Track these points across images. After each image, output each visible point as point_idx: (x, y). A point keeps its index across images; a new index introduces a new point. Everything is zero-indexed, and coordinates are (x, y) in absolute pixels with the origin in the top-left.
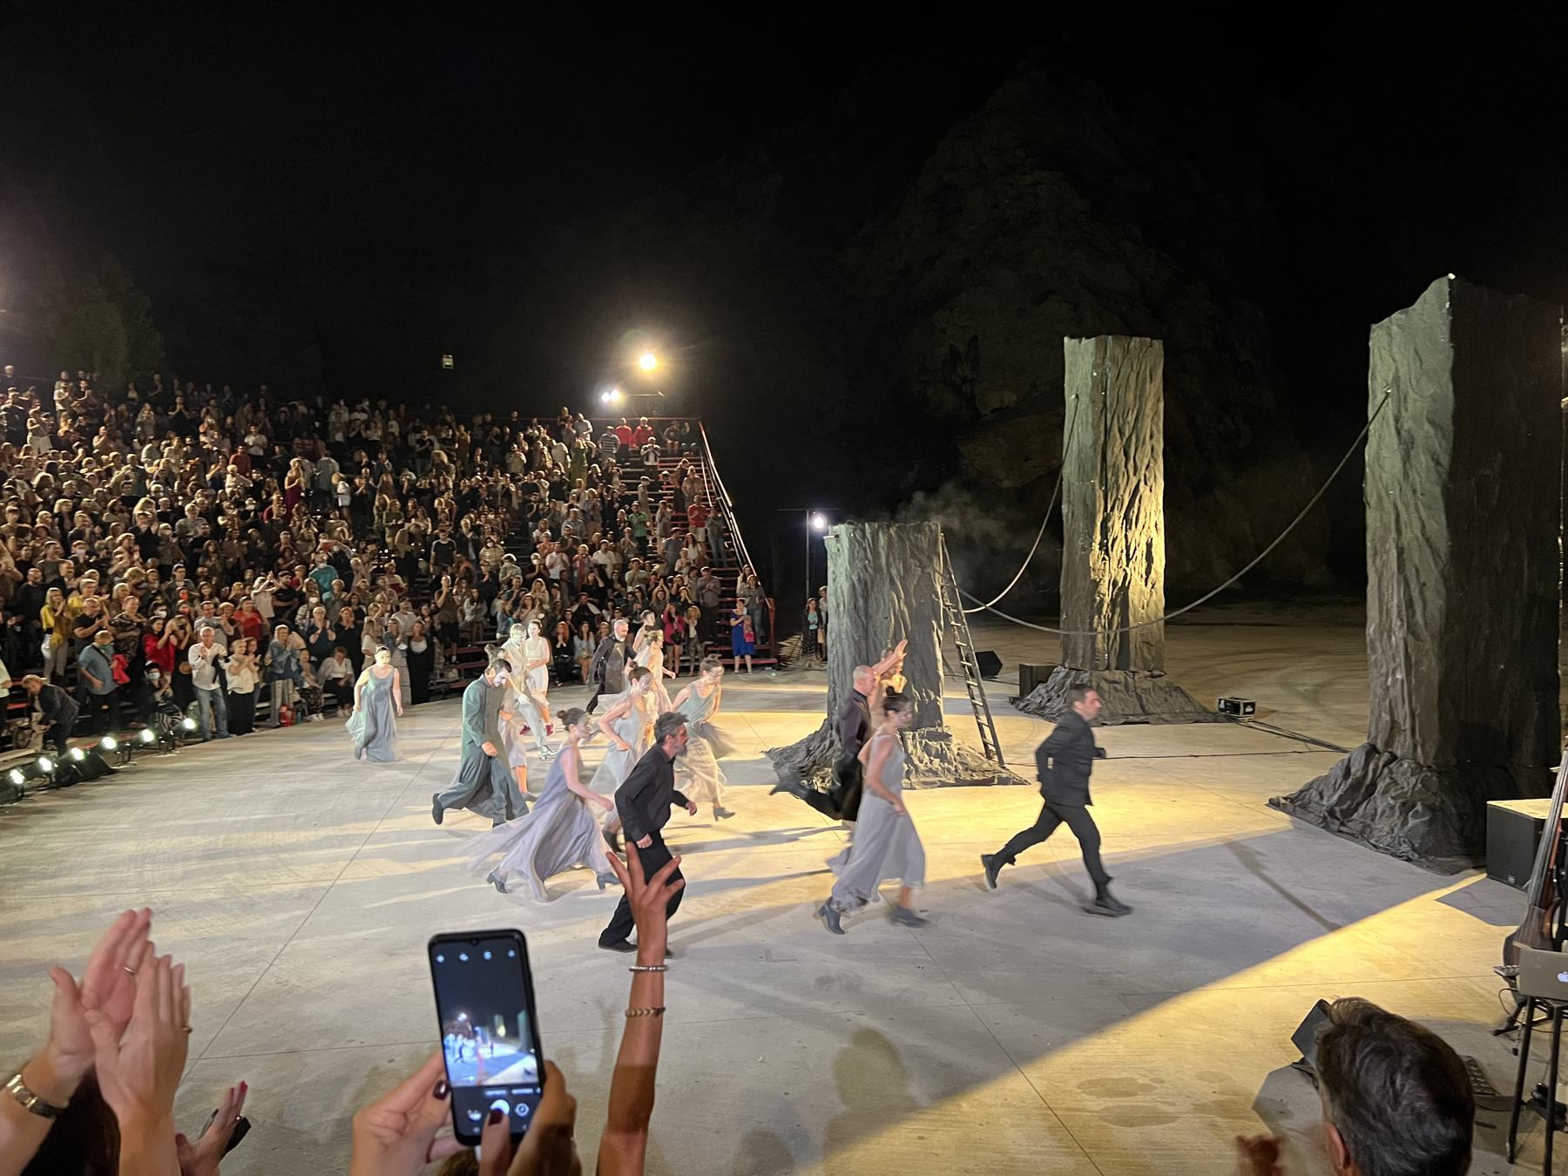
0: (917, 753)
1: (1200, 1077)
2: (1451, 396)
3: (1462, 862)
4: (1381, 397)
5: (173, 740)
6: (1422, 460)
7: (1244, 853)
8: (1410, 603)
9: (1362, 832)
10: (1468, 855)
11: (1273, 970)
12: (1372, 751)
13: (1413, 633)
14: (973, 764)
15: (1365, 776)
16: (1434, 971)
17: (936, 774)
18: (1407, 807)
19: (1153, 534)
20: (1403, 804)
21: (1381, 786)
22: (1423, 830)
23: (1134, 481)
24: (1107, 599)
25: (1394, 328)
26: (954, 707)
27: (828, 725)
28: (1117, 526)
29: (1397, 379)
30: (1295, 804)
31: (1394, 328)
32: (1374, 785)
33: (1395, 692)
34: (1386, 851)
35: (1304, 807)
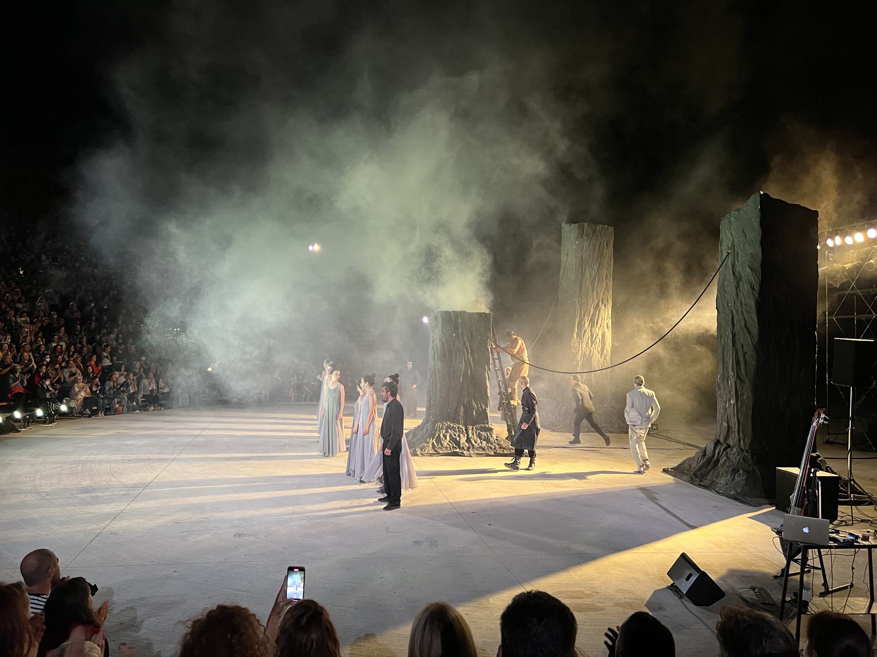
0: (474, 438)
1: (618, 591)
2: (760, 254)
3: (763, 501)
4: (725, 255)
5: (53, 417)
6: (745, 287)
7: (649, 493)
8: (738, 363)
9: (711, 485)
10: (767, 497)
11: (659, 545)
12: (717, 443)
13: (740, 379)
14: (504, 445)
15: (714, 456)
16: (744, 549)
17: (484, 449)
18: (735, 471)
19: (606, 330)
20: (733, 470)
21: (722, 461)
22: (743, 483)
23: (597, 301)
24: (580, 364)
25: (732, 219)
26: (495, 420)
27: (426, 422)
28: (586, 325)
29: (733, 245)
30: (676, 472)
31: (732, 219)
32: (718, 461)
33: (730, 411)
34: (723, 494)
35: (682, 473)
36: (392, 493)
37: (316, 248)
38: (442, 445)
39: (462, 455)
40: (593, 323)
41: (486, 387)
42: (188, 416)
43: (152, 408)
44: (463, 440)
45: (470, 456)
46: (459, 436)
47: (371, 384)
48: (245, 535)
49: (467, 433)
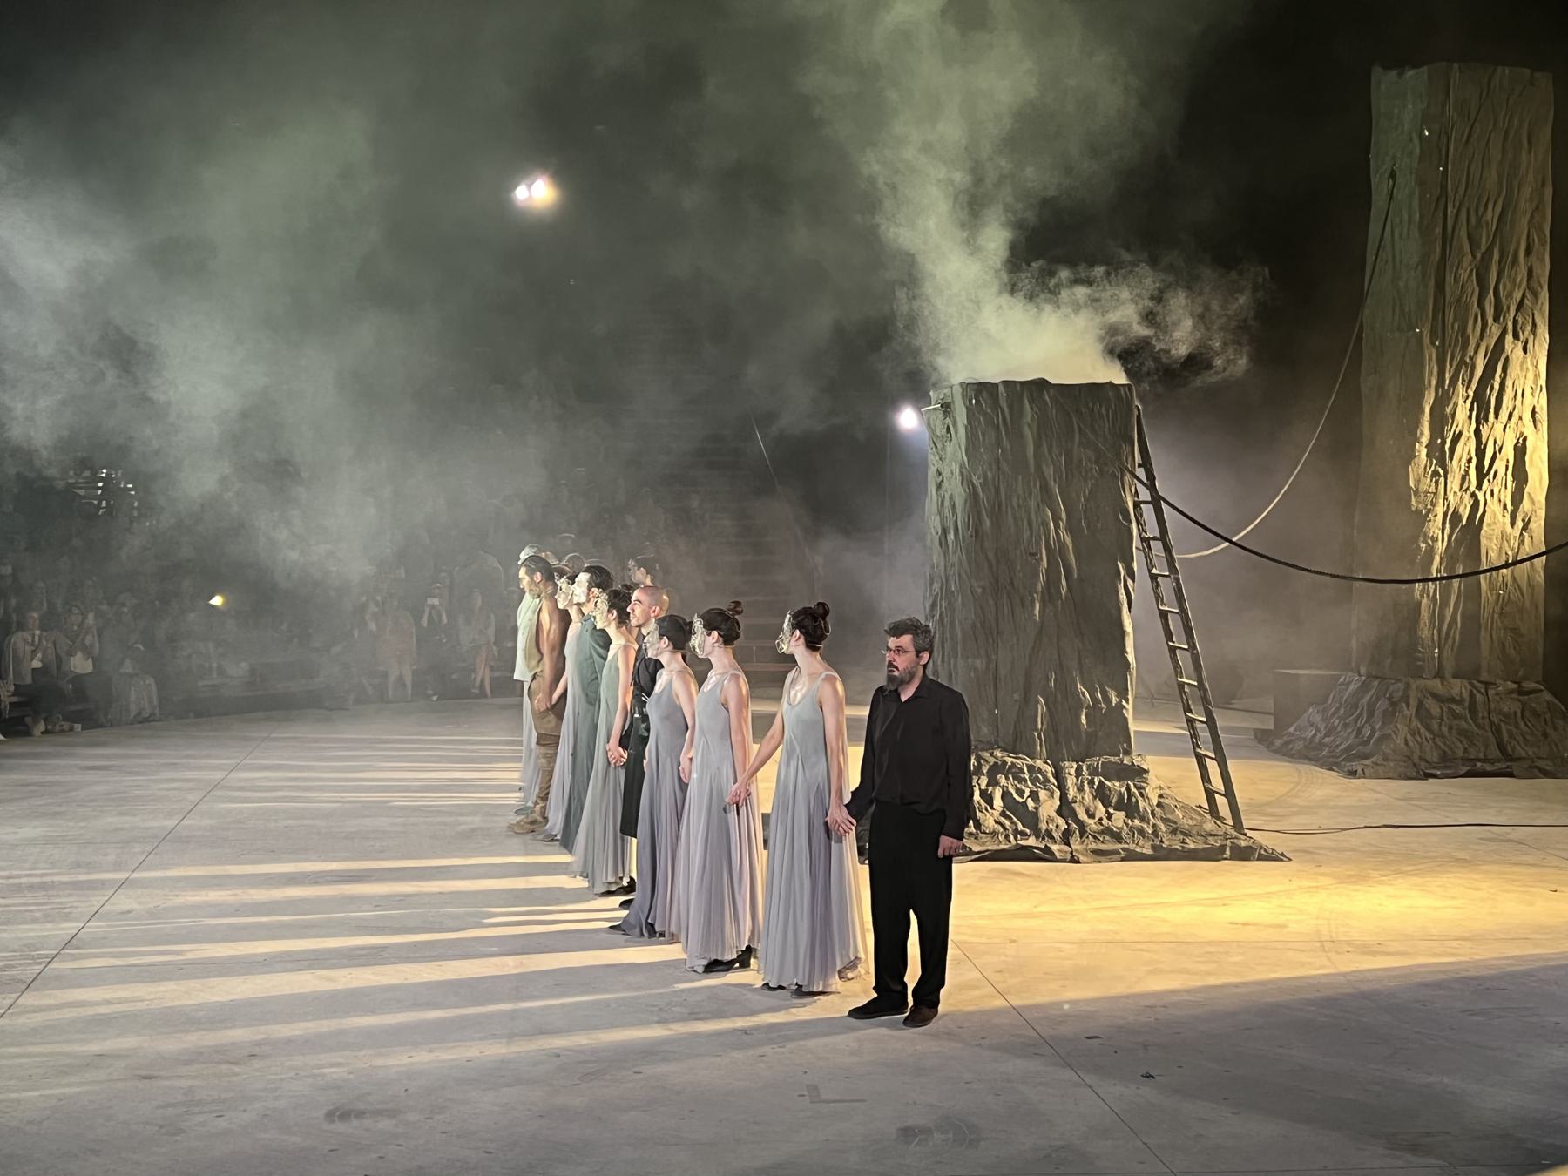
14: (1186, 823)
17: (1117, 837)
19: (1529, 430)
23: (1495, 331)
24: (1441, 547)
26: (1162, 745)
36: (905, 995)
37: (537, 193)
38: (978, 825)
39: (1047, 856)
40: (1482, 408)
41: (1123, 633)
42: (209, 757)
43: (42, 727)
44: (1048, 807)
45: (1074, 860)
46: (1034, 796)
47: (728, 640)
48: (360, 1114)
49: (1061, 786)
